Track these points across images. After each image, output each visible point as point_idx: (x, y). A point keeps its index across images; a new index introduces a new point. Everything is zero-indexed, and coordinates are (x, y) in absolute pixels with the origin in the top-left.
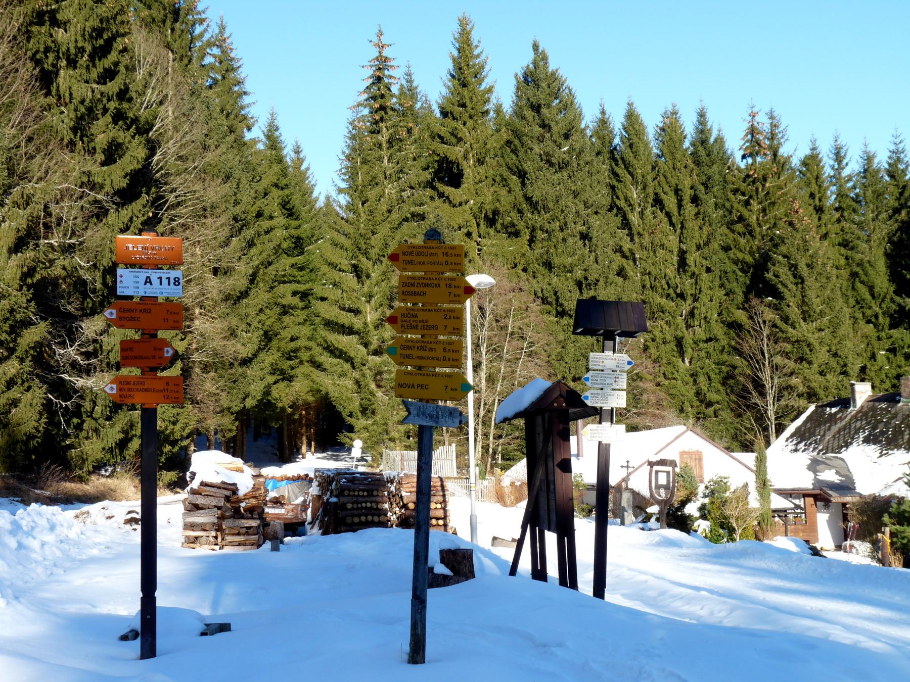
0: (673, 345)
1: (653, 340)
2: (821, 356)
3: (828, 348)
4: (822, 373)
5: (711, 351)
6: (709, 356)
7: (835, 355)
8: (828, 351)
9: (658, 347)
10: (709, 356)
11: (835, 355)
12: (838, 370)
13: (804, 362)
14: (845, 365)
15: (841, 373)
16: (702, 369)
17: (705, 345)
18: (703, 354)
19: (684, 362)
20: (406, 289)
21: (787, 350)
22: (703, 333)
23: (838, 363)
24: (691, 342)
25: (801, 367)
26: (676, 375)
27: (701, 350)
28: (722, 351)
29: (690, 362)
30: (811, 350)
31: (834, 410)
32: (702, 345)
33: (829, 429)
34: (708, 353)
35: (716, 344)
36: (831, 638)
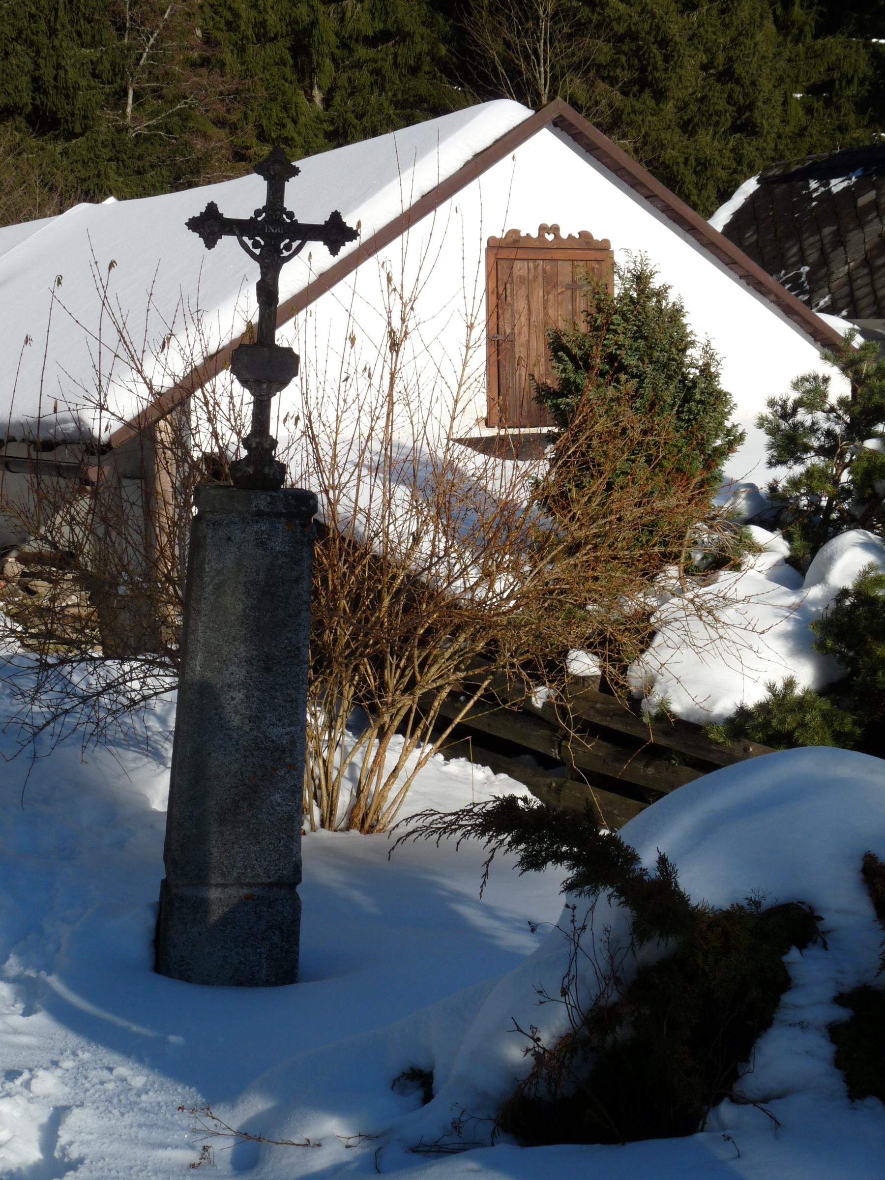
0: (281, 49)
1: (231, 26)
2: (688, 77)
3: (705, 59)
4: (688, 128)
5: (387, 66)
6: (379, 80)
7: (727, 75)
8: (704, 67)
9: (242, 50)
10: (379, 80)
11: (727, 75)
12: (727, 121)
13: (647, 95)
14: (750, 107)
15: (735, 128)
16: (360, 117)
17: (372, 53)
18: (364, 77)
19: (311, 99)
20: (327, 824)
21: (602, 59)
22: (365, 17)
23: (730, 99)
24: (333, 40)
25: (638, 106)
26: (290, 130)
27: (358, 65)
28: (414, 71)
29: (327, 101)
30: (667, 59)
31: (837, 185)
32: (362, 52)
33: (840, 241)
34: (377, 72)
35: (402, 50)
36: (766, 904)
